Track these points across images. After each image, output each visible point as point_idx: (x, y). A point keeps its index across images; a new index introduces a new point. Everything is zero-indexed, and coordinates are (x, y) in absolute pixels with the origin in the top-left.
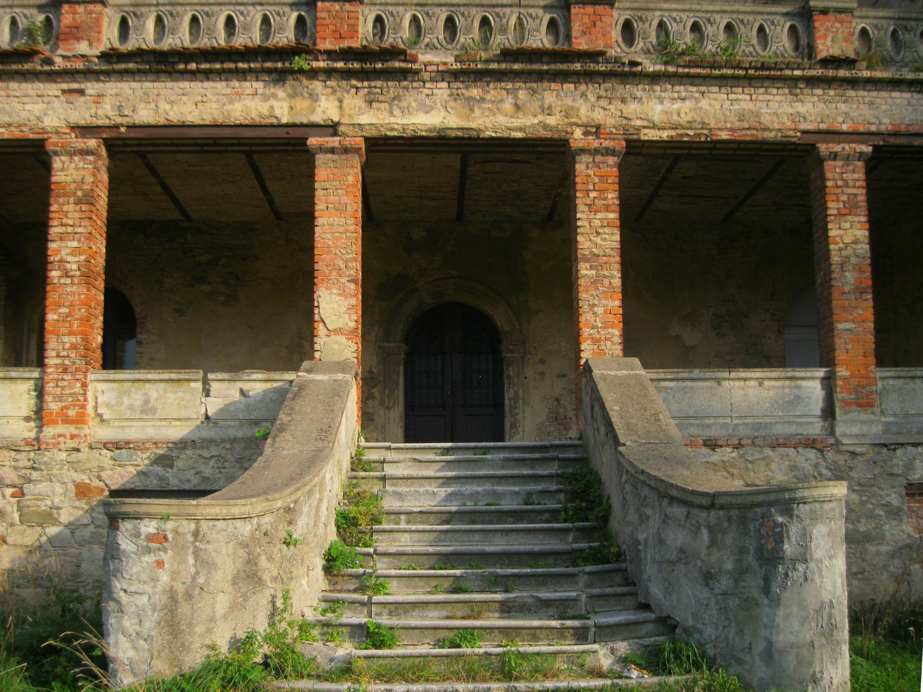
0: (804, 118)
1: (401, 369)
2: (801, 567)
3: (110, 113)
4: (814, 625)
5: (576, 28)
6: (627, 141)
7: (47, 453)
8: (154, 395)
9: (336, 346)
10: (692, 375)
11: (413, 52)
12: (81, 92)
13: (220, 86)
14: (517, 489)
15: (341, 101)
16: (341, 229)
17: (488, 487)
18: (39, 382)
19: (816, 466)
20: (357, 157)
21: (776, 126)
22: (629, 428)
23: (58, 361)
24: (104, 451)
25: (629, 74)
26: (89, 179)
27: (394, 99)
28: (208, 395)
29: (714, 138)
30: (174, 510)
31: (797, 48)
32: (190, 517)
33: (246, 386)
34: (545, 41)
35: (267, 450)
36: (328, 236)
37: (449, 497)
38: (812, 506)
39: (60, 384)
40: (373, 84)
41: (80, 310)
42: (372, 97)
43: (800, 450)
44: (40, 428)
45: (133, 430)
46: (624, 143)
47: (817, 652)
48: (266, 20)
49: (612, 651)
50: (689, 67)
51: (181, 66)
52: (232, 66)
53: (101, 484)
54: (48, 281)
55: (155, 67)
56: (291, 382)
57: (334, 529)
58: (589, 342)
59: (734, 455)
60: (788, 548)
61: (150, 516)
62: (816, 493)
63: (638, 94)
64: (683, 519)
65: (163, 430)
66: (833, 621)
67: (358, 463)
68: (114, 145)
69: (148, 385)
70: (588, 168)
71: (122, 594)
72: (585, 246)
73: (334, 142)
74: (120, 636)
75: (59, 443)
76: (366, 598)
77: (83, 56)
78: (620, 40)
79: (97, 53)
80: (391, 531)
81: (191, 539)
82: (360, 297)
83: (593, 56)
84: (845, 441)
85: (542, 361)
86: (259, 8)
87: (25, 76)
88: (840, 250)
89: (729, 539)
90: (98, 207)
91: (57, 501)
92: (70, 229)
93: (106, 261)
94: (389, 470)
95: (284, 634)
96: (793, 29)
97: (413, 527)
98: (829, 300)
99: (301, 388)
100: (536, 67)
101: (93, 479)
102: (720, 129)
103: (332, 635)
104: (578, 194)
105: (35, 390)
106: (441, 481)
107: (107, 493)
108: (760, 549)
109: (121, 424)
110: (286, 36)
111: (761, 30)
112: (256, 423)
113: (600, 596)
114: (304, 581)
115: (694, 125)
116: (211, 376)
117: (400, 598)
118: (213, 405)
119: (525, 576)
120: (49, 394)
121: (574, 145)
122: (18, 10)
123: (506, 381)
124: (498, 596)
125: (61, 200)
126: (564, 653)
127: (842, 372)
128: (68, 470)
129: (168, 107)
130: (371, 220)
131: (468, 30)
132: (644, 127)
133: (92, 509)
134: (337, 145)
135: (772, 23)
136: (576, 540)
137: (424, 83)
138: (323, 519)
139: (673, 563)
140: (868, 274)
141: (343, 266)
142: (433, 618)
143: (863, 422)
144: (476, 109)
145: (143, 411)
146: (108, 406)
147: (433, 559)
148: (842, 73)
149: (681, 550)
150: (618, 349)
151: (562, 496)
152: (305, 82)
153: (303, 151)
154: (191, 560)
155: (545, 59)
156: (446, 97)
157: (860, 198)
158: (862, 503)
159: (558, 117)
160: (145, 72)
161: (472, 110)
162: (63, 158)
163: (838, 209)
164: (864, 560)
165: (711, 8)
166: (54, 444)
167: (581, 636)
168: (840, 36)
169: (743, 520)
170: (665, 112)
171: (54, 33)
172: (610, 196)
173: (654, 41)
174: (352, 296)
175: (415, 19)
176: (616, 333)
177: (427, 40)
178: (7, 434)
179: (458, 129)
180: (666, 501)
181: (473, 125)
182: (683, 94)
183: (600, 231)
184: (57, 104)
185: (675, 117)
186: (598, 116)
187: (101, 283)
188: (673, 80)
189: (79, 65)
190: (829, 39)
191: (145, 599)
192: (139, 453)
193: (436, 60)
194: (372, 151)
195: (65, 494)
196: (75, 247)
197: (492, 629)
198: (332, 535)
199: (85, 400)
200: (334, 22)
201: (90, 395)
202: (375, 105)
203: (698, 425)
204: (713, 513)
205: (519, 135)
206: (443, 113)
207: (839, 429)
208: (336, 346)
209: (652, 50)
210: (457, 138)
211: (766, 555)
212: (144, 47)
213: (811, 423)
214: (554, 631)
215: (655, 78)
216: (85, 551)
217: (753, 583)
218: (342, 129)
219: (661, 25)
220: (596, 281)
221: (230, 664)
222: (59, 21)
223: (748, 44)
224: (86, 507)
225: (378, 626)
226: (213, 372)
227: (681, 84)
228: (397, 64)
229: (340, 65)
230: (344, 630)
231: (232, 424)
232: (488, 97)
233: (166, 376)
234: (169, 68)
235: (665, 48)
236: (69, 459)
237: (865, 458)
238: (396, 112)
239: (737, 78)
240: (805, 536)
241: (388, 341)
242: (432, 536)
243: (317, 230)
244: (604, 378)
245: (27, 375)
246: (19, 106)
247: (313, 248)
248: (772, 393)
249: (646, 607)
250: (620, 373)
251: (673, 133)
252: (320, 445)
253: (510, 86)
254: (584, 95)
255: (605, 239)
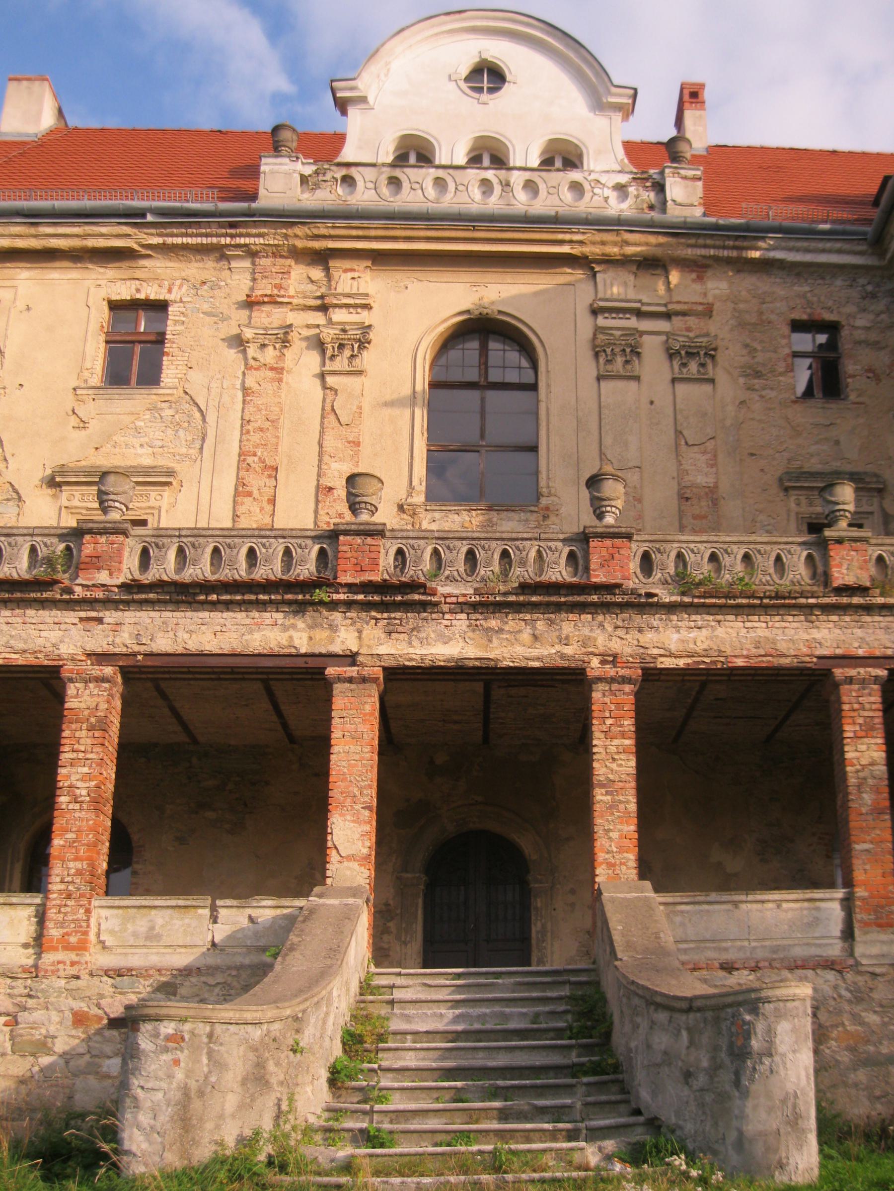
0: (820, 643)
1: (420, 901)
2: (767, 1061)
3: (128, 642)
4: (779, 1113)
5: (595, 560)
6: (643, 669)
7: (44, 980)
8: (160, 921)
9: (348, 873)
10: (709, 899)
11: (434, 585)
12: (100, 620)
13: (240, 616)
14: (524, 1010)
15: (360, 632)
16: (357, 757)
17: (497, 1009)
18: (41, 908)
19: (836, 987)
20: (375, 686)
21: (792, 652)
22: (629, 946)
23: (62, 887)
24: (105, 978)
25: (646, 605)
26: (103, 706)
27: (413, 629)
28: (215, 922)
29: (730, 665)
30: (192, 1013)
31: (814, 576)
32: (207, 1020)
33: (254, 913)
34: (564, 573)
35: (278, 967)
36: (344, 763)
37: (456, 1019)
38: (776, 1004)
39: (63, 910)
40: (393, 615)
41: (87, 835)
42: (391, 628)
43: (818, 971)
44: (39, 955)
45: (136, 957)
46: (640, 671)
47: (783, 1139)
48: (287, 552)
49: (600, 1149)
50: (704, 597)
51: (202, 597)
52: (253, 597)
53: (100, 1012)
54: (56, 806)
55: (175, 597)
56: (301, 908)
57: (340, 1046)
58: (604, 866)
59: (751, 977)
60: (755, 1044)
61: (169, 1018)
62: (779, 992)
63: (655, 623)
64: (666, 1023)
65: (168, 957)
66: (798, 1110)
67: (366, 988)
68: (129, 672)
69: (153, 912)
70: (604, 695)
71: (139, 1090)
72: (601, 772)
73: (352, 671)
74: (135, 1130)
75: (58, 970)
76: (368, 1107)
77: (103, 585)
78: (638, 571)
79: (119, 582)
80: (397, 1049)
81: (205, 1040)
82: (374, 823)
83: (610, 588)
84: (864, 962)
85: (573, 892)
86: (281, 540)
87: (44, 604)
88: (857, 771)
89: (705, 1039)
90: (111, 733)
91: (52, 1029)
92: (81, 755)
93: (116, 787)
94: (398, 994)
95: (287, 1136)
96: (810, 557)
97: (418, 1045)
98: (847, 822)
99: (312, 911)
100: (554, 599)
101: (92, 1007)
102: (735, 656)
103: (334, 1140)
104: (594, 722)
105: (36, 916)
106: (450, 1004)
107: (105, 1021)
108: (731, 1045)
109: (124, 951)
110: (307, 569)
111: (778, 559)
112: (264, 949)
113: (595, 1104)
114: (309, 1089)
115: (711, 653)
116: (219, 903)
117: (401, 1107)
118: (221, 932)
119: (525, 1087)
120: (51, 920)
121: (590, 673)
122: (38, 539)
123: (533, 913)
124: (497, 1104)
125: (74, 726)
126: (551, 1150)
127: (860, 892)
128: (66, 998)
129: (186, 636)
130: (390, 744)
131: (489, 563)
132: (661, 656)
133: (89, 1038)
134: (355, 674)
135: (789, 552)
136: (579, 1056)
137: (443, 614)
138: (329, 1033)
139: (658, 1065)
140: (886, 795)
141: (358, 793)
142: (433, 1124)
143: (883, 942)
144: (494, 640)
145: (147, 938)
146: (112, 932)
147: (436, 1074)
148: (856, 600)
149: (665, 1053)
150: (633, 874)
151: (569, 1017)
152: (325, 613)
153: (319, 680)
154: (205, 1060)
155: (562, 592)
156: (464, 628)
157: (877, 721)
158: (885, 1024)
159: (575, 647)
160: (165, 602)
161: (490, 641)
162: (77, 685)
163: (855, 732)
164: (887, 1083)
165: (728, 539)
166: (53, 972)
167: (572, 1136)
168: (855, 564)
169: (717, 1020)
170: (682, 641)
171: (74, 561)
172: (626, 723)
173: (672, 572)
174: (365, 822)
175: (436, 552)
176: (631, 857)
177: (447, 573)
178: (4, 960)
179: (476, 659)
180: (652, 1007)
181: (491, 655)
182: (700, 623)
183: (616, 757)
184: (74, 631)
185: (692, 646)
186: (615, 645)
187: (109, 809)
188: (689, 610)
189: (99, 594)
190: (845, 566)
191: (160, 1095)
192: (141, 980)
193: (456, 592)
194: (391, 680)
195: (61, 1023)
196: (85, 772)
197: (487, 1132)
198: (337, 1050)
199: (88, 926)
200: (355, 555)
201: (93, 921)
202: (394, 635)
203: (715, 948)
204: (692, 1016)
205: (536, 664)
206: (461, 644)
207: (859, 950)
208: (348, 873)
209: (670, 581)
210: (474, 668)
211: (736, 1051)
212: (165, 578)
213: (831, 944)
214: (547, 1134)
215: (671, 608)
216: (79, 1083)
217: (725, 1078)
218: (360, 659)
219: (680, 556)
220: (612, 807)
221: (237, 1159)
222: (80, 551)
223: (765, 572)
224: (83, 1036)
225: (379, 1130)
226: (221, 898)
227: (697, 614)
228: (417, 597)
229: (361, 597)
230: (346, 1135)
231: (239, 950)
232: (506, 628)
233: (173, 902)
234: (190, 599)
235: (683, 579)
236: (68, 987)
237: (886, 978)
238: (415, 642)
239: (753, 606)
240: (770, 1032)
241: (407, 872)
242: (436, 1054)
243: (332, 757)
244: (613, 900)
245: (28, 901)
246: (36, 633)
247: (327, 774)
248: (790, 915)
249: (638, 1112)
250: (629, 896)
251: (689, 661)
252: (329, 962)
253: (528, 617)
254: (601, 625)
255: (620, 765)
